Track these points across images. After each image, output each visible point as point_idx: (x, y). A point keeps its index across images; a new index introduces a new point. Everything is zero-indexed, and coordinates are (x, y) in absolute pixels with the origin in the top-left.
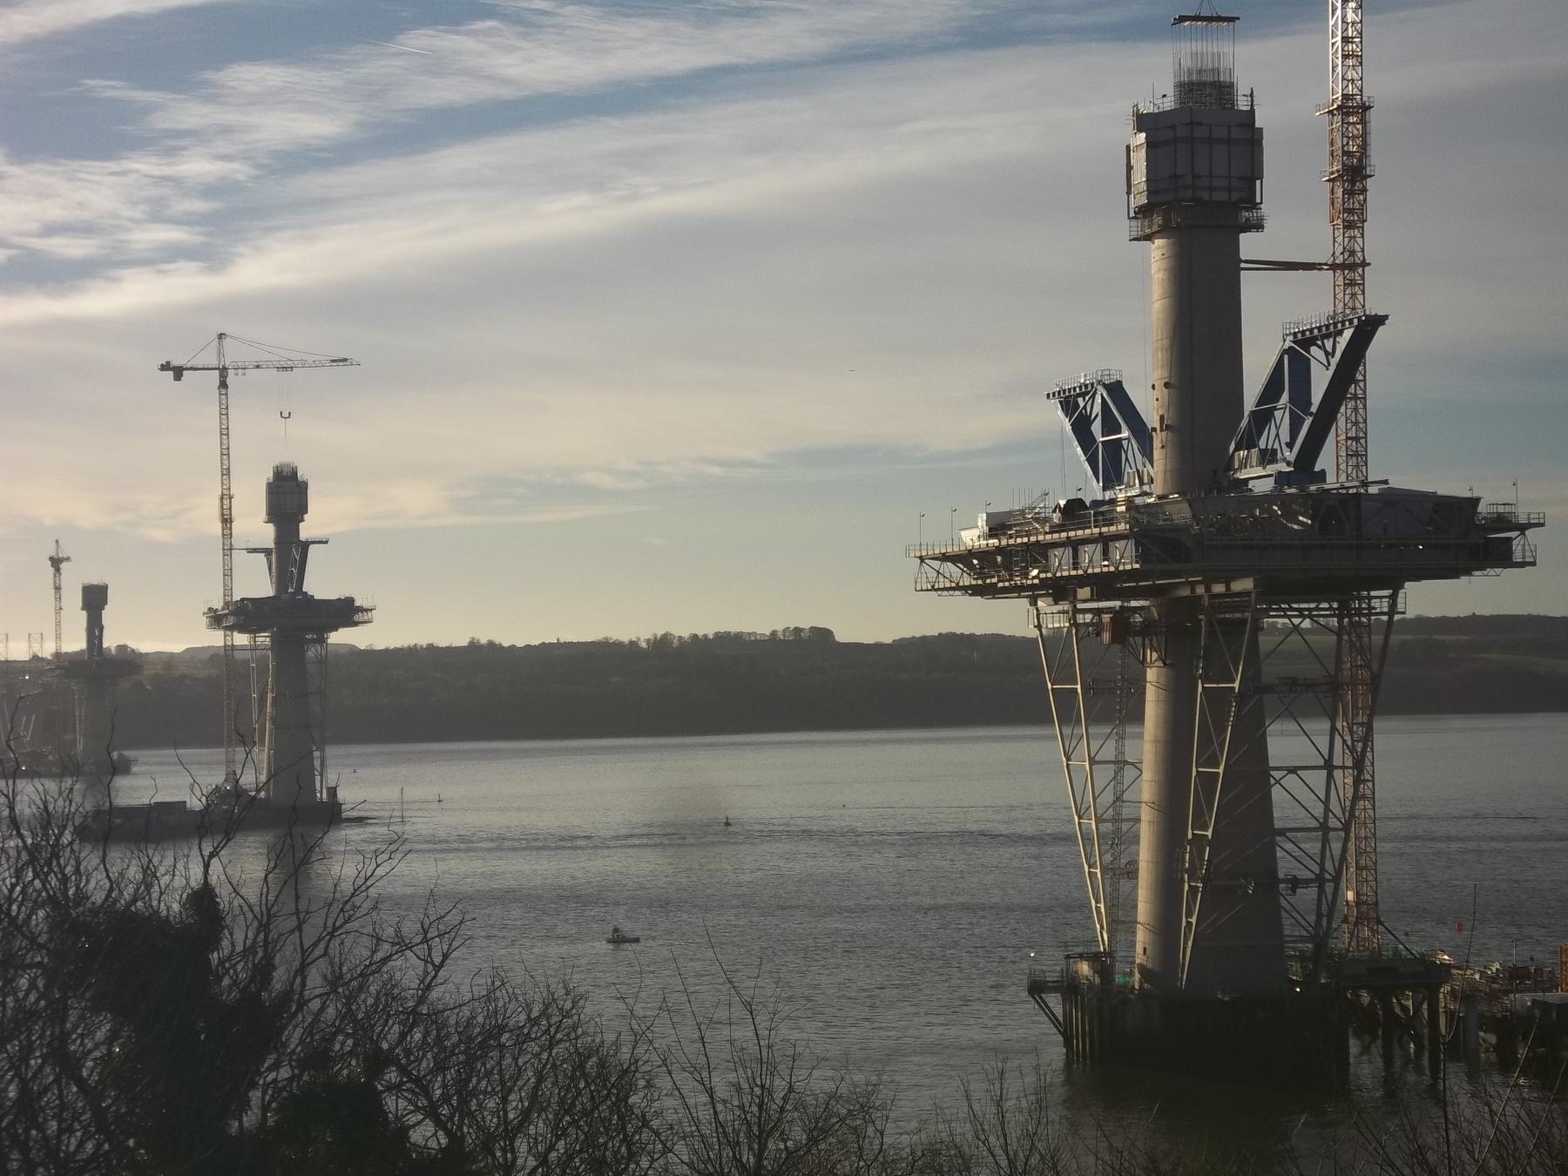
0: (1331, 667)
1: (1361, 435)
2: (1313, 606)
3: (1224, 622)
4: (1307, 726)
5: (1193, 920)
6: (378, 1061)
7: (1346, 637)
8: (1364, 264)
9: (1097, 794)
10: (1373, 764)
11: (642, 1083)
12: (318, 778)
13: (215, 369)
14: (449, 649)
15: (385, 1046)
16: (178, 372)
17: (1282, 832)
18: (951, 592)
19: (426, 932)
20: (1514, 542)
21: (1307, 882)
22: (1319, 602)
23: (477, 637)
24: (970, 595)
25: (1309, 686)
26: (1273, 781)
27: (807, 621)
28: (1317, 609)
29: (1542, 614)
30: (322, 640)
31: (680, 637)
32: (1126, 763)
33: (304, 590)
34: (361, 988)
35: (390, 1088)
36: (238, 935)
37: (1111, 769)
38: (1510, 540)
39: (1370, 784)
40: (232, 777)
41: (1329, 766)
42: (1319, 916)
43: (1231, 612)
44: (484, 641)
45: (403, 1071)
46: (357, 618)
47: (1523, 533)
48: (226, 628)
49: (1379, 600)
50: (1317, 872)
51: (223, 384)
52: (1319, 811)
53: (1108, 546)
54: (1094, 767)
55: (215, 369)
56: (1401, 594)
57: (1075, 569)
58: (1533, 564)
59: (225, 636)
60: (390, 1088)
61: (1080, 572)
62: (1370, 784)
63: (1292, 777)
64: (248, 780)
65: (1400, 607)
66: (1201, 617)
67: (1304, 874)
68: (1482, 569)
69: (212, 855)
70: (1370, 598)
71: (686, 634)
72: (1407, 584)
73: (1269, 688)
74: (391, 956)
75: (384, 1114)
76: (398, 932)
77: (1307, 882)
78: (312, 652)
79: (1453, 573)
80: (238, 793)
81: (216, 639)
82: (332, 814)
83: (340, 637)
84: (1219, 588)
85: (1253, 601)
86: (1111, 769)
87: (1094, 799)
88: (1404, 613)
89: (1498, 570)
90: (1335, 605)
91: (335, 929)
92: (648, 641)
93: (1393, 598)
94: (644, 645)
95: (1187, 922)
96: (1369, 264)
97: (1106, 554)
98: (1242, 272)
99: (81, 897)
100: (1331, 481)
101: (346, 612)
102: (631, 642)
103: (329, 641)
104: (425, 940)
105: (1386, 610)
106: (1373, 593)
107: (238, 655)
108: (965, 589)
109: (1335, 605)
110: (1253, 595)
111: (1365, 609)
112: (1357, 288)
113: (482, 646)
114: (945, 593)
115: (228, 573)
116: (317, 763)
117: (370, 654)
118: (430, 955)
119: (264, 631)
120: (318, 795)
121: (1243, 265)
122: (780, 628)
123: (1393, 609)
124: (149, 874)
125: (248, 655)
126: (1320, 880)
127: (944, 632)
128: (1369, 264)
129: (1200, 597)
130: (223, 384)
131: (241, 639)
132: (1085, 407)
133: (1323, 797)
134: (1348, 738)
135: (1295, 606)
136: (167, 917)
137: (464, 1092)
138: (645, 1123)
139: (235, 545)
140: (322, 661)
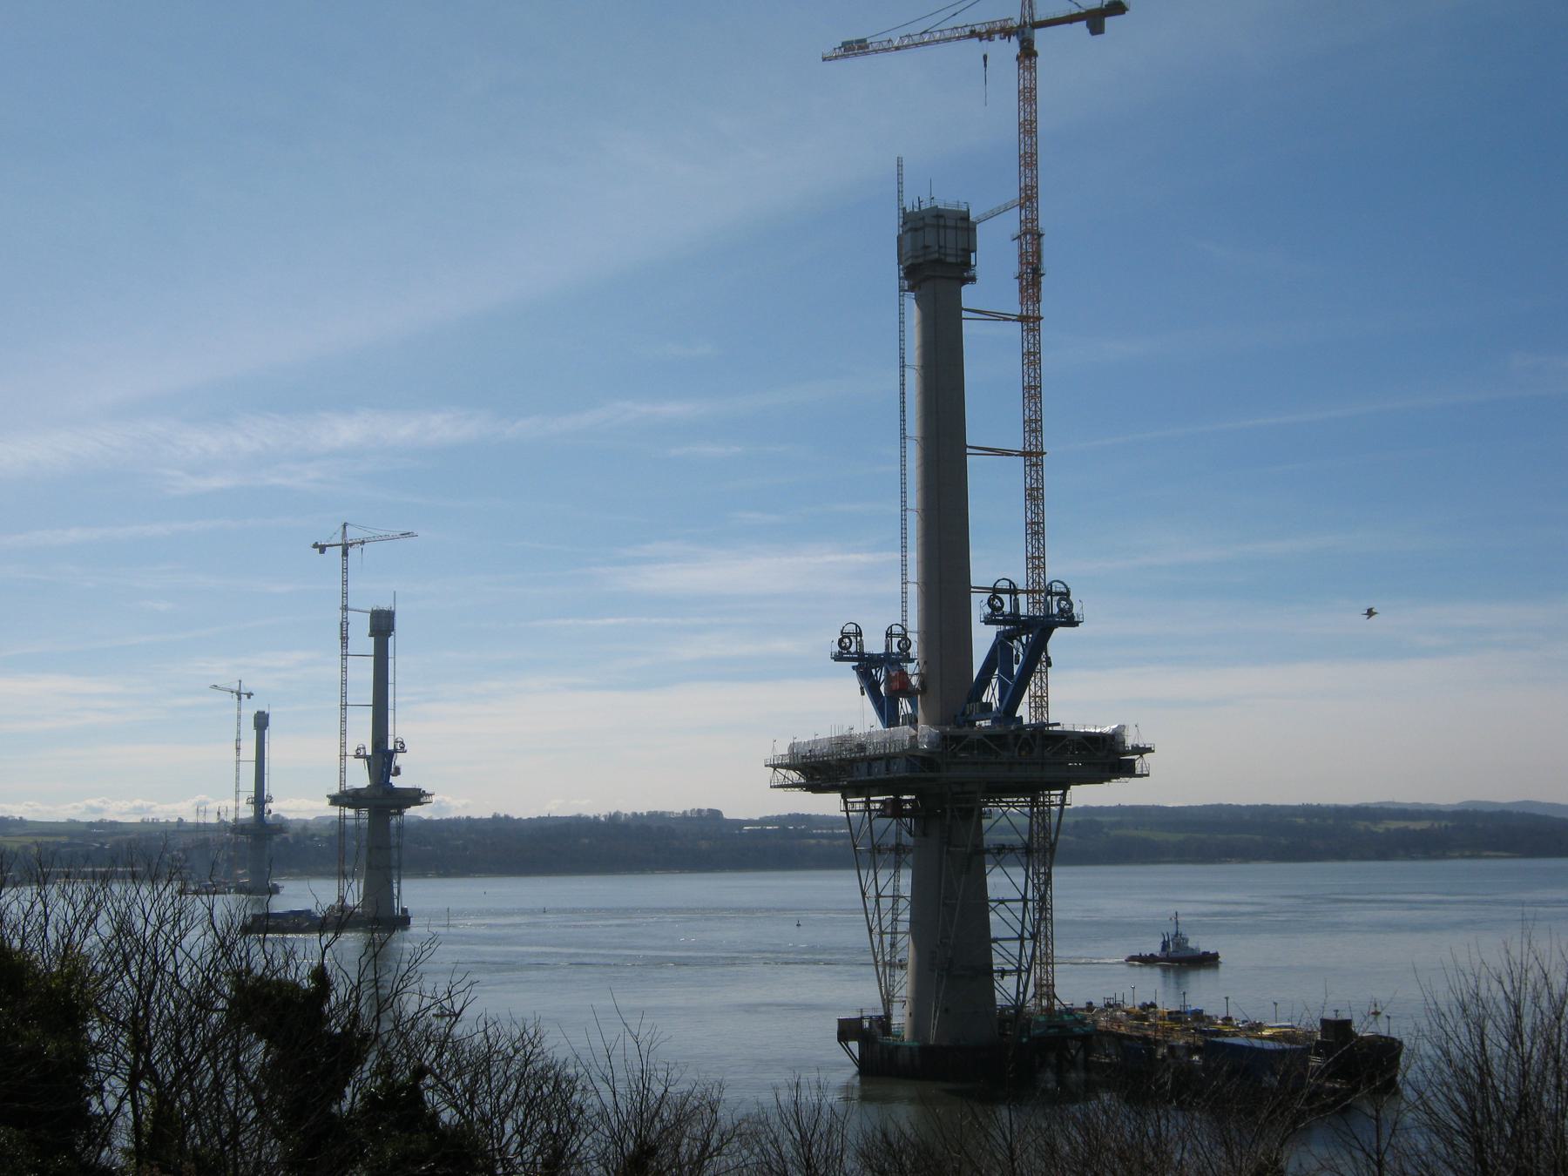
0: (1026, 837)
1: (1045, 694)
2: (1015, 799)
4: (1008, 870)
6: (421, 1072)
7: (1035, 819)
11: (580, 1088)
12: (396, 901)
13: (340, 545)
14: (480, 819)
15: (427, 1063)
16: (322, 549)
17: (996, 940)
19: (450, 993)
20: (1136, 762)
21: (1010, 972)
23: (498, 812)
25: (1012, 849)
26: (990, 909)
27: (705, 806)
28: (1017, 802)
29: (1161, 805)
30: (400, 813)
31: (626, 815)
32: (900, 897)
33: (390, 781)
34: (413, 1027)
35: (428, 1087)
36: (340, 992)
38: (1134, 760)
40: (342, 899)
42: (1018, 993)
44: (502, 815)
45: (438, 1078)
46: (422, 800)
47: (1141, 756)
49: (1055, 796)
51: (345, 553)
52: (1018, 928)
55: (340, 545)
56: (1068, 792)
57: (869, 775)
58: (1147, 775)
59: (340, 810)
60: (428, 1087)
63: (1002, 906)
64: (350, 902)
65: (1068, 801)
67: (1008, 967)
69: (326, 947)
71: (629, 812)
72: (1072, 787)
73: (988, 851)
74: (430, 1007)
75: (424, 1103)
76: (1128, 1145)
77: (1010, 972)
78: (394, 821)
79: (1100, 780)
80: (343, 908)
81: (335, 812)
82: (403, 921)
83: (412, 812)
89: (1127, 779)
90: (1029, 799)
91: (397, 992)
92: (605, 816)
93: (1064, 795)
94: (603, 819)
98: (972, 594)
99: (249, 971)
100: (1026, 721)
101: (415, 797)
102: (595, 817)
104: (449, 997)
105: (1059, 803)
106: (1052, 792)
109: (1029, 799)
113: (501, 818)
115: (343, 771)
116: (395, 891)
117: (429, 822)
118: (452, 1007)
120: (396, 911)
121: (972, 590)
122: (689, 809)
124: (290, 955)
127: (792, 813)
134: (1036, 881)
136: (897, 867)
137: (471, 1090)
138: (581, 1111)
140: (400, 827)
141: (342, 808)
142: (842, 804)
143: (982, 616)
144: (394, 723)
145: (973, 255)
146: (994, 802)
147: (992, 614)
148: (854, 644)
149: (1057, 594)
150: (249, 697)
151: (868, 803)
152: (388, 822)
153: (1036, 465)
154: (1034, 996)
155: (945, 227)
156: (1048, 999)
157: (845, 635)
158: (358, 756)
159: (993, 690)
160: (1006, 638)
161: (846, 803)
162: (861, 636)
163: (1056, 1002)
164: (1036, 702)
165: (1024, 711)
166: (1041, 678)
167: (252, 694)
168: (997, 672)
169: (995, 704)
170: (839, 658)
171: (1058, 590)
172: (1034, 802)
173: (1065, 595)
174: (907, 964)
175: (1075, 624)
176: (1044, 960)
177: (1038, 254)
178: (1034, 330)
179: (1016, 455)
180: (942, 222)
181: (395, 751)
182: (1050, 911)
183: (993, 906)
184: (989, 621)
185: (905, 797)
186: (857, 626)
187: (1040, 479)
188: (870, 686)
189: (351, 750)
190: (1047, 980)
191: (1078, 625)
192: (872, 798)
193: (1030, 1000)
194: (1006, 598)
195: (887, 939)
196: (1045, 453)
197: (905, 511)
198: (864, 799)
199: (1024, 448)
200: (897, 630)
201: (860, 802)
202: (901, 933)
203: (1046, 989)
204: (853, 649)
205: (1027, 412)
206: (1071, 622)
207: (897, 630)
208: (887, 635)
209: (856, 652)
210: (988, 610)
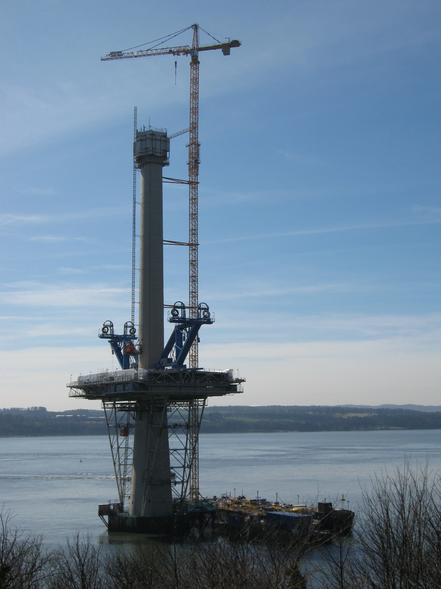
2: (182, 403)
24: (85, 398)
41: (186, 449)
42: (182, 492)
54: (120, 449)
56: (207, 400)
57: (115, 392)
58: (242, 392)
62: (197, 262)
65: (206, 404)
66: (151, 406)
72: (208, 397)
73: (169, 427)
88: (207, 405)
89: (233, 394)
93: (204, 401)
111: (197, 404)
121: (164, 306)
126: (183, 482)
142: (102, 405)
143: (169, 319)
145: (168, 153)
147: (173, 318)
149: (203, 309)
151: (114, 404)
154: (190, 494)
155: (156, 140)
156: (196, 495)
157: (105, 326)
161: (104, 404)
162: (113, 327)
163: (200, 496)
164: (192, 359)
166: (195, 363)
169: (174, 359)
170: (102, 337)
171: (203, 307)
176: (194, 477)
177: (197, 154)
178: (195, 188)
180: (154, 137)
184: (172, 321)
186: (111, 322)
187: (196, 256)
188: (117, 350)
190: (196, 486)
192: (116, 402)
194: (180, 310)
198: (113, 403)
200: (129, 324)
203: (195, 491)
204: (109, 333)
206: (209, 322)
207: (129, 324)
208: (125, 327)
209: (110, 335)
210: (171, 316)
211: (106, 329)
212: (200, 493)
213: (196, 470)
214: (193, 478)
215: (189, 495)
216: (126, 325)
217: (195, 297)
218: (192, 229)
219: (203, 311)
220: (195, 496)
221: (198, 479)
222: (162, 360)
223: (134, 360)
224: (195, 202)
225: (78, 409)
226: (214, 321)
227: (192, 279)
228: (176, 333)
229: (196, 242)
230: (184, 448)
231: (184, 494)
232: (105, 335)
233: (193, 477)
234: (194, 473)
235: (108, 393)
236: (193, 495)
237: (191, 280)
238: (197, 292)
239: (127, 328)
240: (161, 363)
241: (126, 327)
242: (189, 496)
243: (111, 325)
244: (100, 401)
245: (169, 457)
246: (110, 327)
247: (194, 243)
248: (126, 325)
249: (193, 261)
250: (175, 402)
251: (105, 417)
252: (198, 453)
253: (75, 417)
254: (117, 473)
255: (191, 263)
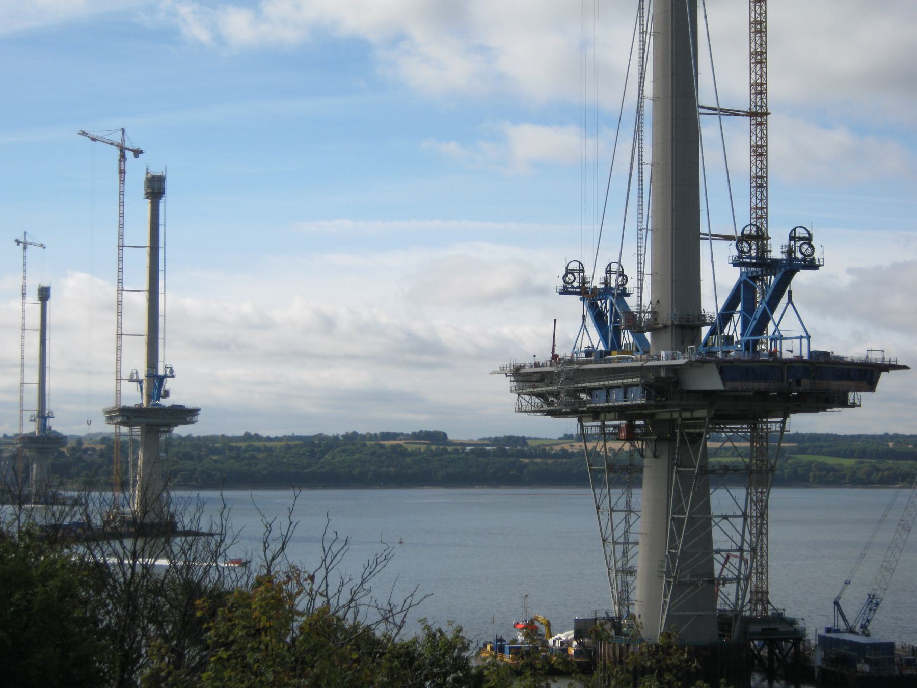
2: (739, 426)
3: (689, 434)
4: (728, 487)
5: (668, 600)
8: (767, 114)
9: (614, 527)
10: (767, 546)
18: (535, 414)
22: (743, 424)
23: (249, 431)
24: (545, 415)
26: (713, 524)
30: (170, 431)
37: (623, 514)
39: (765, 148)
41: (745, 516)
42: (737, 599)
43: (694, 428)
48: (116, 423)
49: (773, 424)
50: (737, 575)
51: (25, 248)
53: (627, 390)
54: (613, 513)
56: (788, 420)
57: (607, 402)
58: (859, 406)
61: (611, 404)
62: (765, 148)
65: (787, 428)
66: (676, 431)
68: (831, 408)
70: (767, 422)
72: (791, 416)
73: (713, 472)
83: (181, 430)
84: (687, 415)
85: (706, 423)
86: (623, 514)
87: (613, 531)
88: (789, 431)
89: (840, 409)
92: (343, 436)
93: (784, 422)
95: (664, 601)
96: (770, 238)
97: (625, 397)
101: (185, 414)
103: (174, 432)
105: (779, 429)
106: (769, 420)
107: (122, 439)
108: (542, 412)
110: (707, 420)
111: (765, 428)
112: (763, 157)
114: (532, 414)
119: (137, 425)
121: (701, 236)
123: (783, 428)
125: (127, 438)
126: (738, 579)
128: (770, 238)
129: (676, 420)
130: (25, 248)
131: (124, 429)
132: (601, 307)
133: (741, 532)
135: (728, 426)
139: (123, 377)
140: (169, 443)
141: (118, 426)
142: (579, 427)
143: (730, 258)
144: (164, 348)
146: (720, 428)
148: (577, 280)
149: (800, 239)
150: (136, 156)
151: (603, 427)
152: (158, 438)
153: (761, 124)
154: (750, 602)
156: (763, 605)
157: (569, 272)
158: (131, 380)
159: (735, 326)
160: (750, 278)
161: (582, 427)
163: (770, 607)
165: (764, 347)
167: (141, 152)
168: (739, 308)
169: (737, 337)
170: (564, 292)
171: (801, 235)
172: (754, 429)
173: (808, 240)
174: (636, 571)
175: (815, 267)
176: (759, 570)
179: (743, 115)
181: (165, 376)
182: (765, 526)
183: (717, 521)
185: (638, 422)
186: (580, 263)
187: (764, 137)
188: (599, 318)
189: (126, 375)
190: (762, 588)
191: (818, 269)
192: (607, 423)
193: (747, 605)
195: (619, 548)
196: (770, 113)
197: (642, 164)
198: (599, 423)
199: (750, 108)
200: (615, 267)
201: (595, 426)
202: (631, 543)
203: (761, 596)
204: (576, 284)
205: (753, 76)
206: (811, 265)
207: (615, 267)
208: (607, 272)
209: (578, 287)
211: (569, 276)
212: (771, 600)
213: (762, 556)
214: (757, 573)
215: (749, 605)
216: (608, 269)
217: (761, 217)
218: (756, 83)
219: (798, 243)
220: (760, 607)
221: (767, 574)
222: (712, 338)
223: (631, 337)
224: (761, 28)
225: (505, 435)
226: (821, 264)
227: (756, 183)
228: (742, 286)
229: (764, 108)
230: (740, 513)
231: (740, 602)
232: (569, 288)
233: (757, 570)
234: (759, 563)
235: (592, 405)
236: (756, 604)
237: (754, 184)
238: (767, 208)
239: (610, 274)
240: (710, 344)
241: (609, 272)
242: (748, 607)
243: (581, 268)
244: (574, 420)
245: (710, 532)
246: (579, 273)
247: (759, 111)
248: (608, 269)
249: (757, 146)
250: (724, 424)
251: (777, 444)
252: (767, 524)
253: (502, 453)
254: (608, 558)
255: (755, 151)
